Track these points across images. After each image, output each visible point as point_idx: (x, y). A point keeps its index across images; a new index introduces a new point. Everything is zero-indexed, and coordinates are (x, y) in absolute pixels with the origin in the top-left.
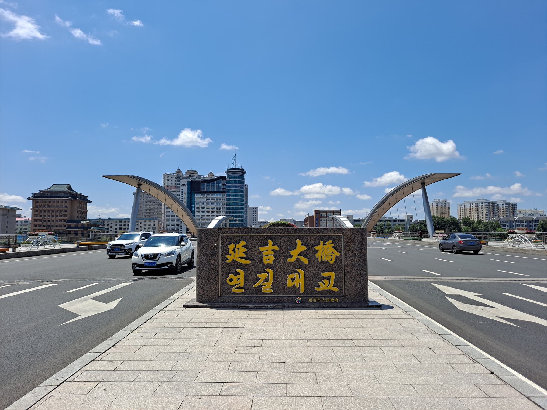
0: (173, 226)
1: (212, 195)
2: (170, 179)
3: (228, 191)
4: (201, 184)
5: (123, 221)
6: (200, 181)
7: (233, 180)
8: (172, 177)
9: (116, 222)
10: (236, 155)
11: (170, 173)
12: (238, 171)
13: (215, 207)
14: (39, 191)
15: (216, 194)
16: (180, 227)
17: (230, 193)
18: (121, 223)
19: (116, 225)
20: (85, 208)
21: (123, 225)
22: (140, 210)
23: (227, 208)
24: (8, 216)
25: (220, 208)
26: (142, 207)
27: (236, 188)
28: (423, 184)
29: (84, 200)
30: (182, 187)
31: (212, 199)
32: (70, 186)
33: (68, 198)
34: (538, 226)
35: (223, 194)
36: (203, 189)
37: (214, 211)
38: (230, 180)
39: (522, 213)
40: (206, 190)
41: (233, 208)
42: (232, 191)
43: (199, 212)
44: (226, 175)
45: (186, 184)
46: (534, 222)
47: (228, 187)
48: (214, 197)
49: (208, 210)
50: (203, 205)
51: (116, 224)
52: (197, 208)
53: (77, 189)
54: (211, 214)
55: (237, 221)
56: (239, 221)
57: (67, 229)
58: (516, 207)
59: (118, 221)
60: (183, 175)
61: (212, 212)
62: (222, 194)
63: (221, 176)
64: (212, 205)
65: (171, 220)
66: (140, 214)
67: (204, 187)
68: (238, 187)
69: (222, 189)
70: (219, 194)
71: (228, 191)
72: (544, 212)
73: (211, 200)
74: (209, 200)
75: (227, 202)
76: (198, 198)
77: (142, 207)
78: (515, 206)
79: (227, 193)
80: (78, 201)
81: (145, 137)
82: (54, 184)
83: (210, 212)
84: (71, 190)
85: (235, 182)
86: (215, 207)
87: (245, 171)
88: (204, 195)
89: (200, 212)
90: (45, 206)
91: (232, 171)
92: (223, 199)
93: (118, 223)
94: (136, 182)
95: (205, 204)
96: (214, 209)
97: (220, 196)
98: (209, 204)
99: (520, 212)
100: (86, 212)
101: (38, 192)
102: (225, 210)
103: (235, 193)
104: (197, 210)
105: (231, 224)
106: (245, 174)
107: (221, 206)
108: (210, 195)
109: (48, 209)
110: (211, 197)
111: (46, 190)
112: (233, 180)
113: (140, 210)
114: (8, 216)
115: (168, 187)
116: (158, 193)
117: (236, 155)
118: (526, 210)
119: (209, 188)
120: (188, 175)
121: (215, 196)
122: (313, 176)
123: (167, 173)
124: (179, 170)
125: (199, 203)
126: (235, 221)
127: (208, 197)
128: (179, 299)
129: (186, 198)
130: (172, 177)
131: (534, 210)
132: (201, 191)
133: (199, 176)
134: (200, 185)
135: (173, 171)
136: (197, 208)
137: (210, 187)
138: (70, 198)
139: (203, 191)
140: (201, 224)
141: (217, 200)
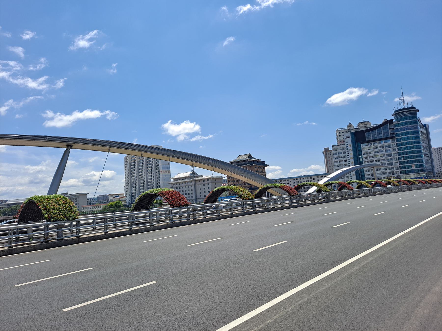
1: (380, 143)
2: (341, 134)
3: (398, 135)
4: (366, 133)
5: (286, 180)
6: (364, 130)
7: (402, 122)
8: (343, 132)
9: (294, 180)
10: (402, 93)
11: (341, 129)
12: (406, 110)
13: (384, 155)
15: (383, 141)
18: (297, 181)
19: (294, 183)
20: (264, 171)
22: (330, 166)
23: (399, 154)
24: (215, 184)
25: (391, 155)
26: (331, 163)
29: (262, 165)
30: (346, 140)
31: (380, 147)
32: (250, 155)
33: (247, 165)
35: (393, 139)
37: (384, 158)
38: (399, 122)
40: (372, 138)
41: (407, 153)
42: (403, 134)
43: (368, 162)
47: (398, 130)
48: (383, 144)
50: (371, 154)
51: (294, 181)
52: (365, 158)
53: (257, 156)
54: (381, 162)
55: (414, 167)
56: (416, 166)
59: (295, 179)
60: (354, 128)
61: (382, 160)
62: (391, 140)
64: (381, 153)
66: (330, 170)
69: (391, 134)
71: (398, 135)
74: (377, 148)
75: (398, 147)
76: (365, 148)
77: (331, 163)
79: (396, 138)
81: (58, 84)
82: (240, 155)
83: (380, 160)
84: (251, 158)
85: (406, 124)
86: (384, 155)
87: (417, 109)
88: (370, 144)
89: (369, 161)
91: (403, 111)
92: (393, 145)
93: (295, 181)
94: (65, 144)
95: (373, 153)
96: (384, 157)
98: (377, 152)
100: (265, 174)
102: (397, 157)
104: (366, 160)
105: (407, 171)
107: (392, 152)
108: (377, 143)
110: (378, 144)
111: (234, 161)
112: (402, 122)
113: (330, 166)
114: (215, 184)
115: (340, 142)
117: (402, 93)
120: (359, 127)
121: (383, 143)
123: (338, 129)
124: (350, 124)
125: (366, 153)
126: (411, 167)
127: (375, 145)
129: (352, 150)
130: (343, 132)
132: (366, 140)
133: (372, 126)
135: (345, 126)
136: (365, 158)
137: (376, 135)
138: (248, 164)
141: (386, 146)
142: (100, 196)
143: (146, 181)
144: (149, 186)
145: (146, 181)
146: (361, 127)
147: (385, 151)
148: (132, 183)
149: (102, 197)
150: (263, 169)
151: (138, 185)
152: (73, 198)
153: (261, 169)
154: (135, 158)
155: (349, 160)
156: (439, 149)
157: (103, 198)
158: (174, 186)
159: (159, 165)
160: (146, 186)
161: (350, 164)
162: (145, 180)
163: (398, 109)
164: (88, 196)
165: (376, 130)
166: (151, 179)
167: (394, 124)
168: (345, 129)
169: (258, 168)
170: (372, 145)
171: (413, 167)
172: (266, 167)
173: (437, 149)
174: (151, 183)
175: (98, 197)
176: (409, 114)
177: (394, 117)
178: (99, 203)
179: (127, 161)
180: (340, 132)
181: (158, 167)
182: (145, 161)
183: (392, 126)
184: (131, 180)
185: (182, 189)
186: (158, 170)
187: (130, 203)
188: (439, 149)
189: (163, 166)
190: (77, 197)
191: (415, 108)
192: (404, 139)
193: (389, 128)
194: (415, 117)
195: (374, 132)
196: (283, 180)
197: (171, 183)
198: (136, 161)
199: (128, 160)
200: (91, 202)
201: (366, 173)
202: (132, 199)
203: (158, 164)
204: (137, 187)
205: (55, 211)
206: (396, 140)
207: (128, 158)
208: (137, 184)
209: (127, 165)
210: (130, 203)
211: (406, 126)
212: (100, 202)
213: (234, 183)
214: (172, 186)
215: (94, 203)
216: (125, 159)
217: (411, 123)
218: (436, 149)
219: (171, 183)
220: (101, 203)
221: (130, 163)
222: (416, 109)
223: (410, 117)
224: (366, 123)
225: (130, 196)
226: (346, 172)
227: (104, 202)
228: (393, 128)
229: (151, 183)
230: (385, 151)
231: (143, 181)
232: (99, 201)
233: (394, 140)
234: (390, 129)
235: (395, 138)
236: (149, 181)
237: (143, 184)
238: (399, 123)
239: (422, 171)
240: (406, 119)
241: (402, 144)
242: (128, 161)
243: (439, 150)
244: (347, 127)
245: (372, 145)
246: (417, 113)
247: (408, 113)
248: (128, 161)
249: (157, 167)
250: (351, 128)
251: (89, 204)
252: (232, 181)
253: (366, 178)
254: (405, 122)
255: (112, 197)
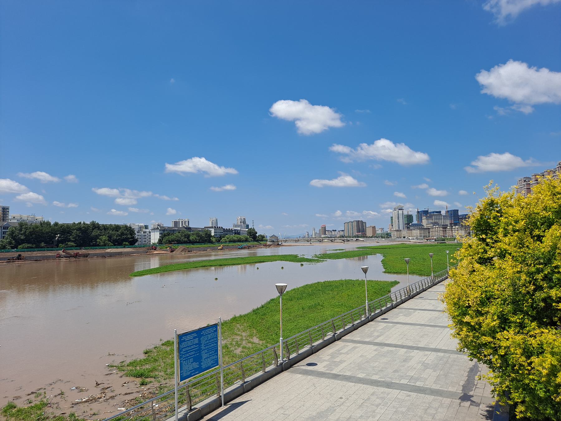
34: (7, 233)
39: (16, 219)
46: (3, 229)
49: (338, 409)
58: (8, 212)
72: (42, 218)
78: (7, 210)
79: (524, 306)
99: (14, 217)
118: (21, 216)
128: (19, 386)
131: (31, 216)
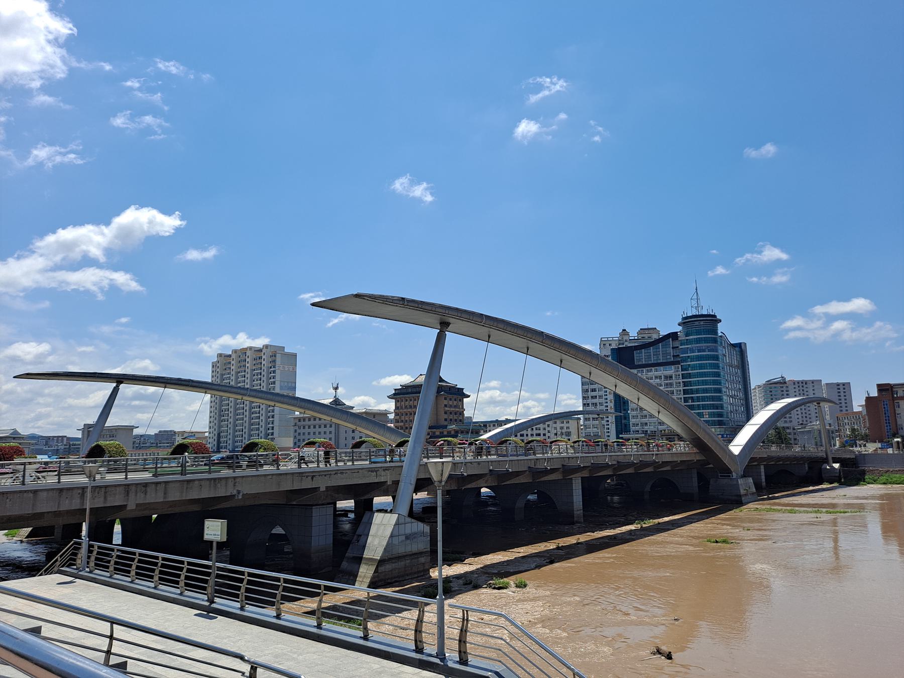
0: (596, 429)
3: (685, 360)
4: (635, 352)
6: (632, 346)
7: (691, 337)
10: (696, 289)
11: (608, 338)
12: (699, 319)
14: (401, 386)
15: (662, 368)
16: (606, 431)
17: (688, 363)
20: (460, 406)
21: (542, 429)
27: (698, 352)
28: (444, 326)
31: (656, 377)
35: (677, 366)
36: (640, 360)
38: (687, 338)
40: (645, 361)
42: (692, 359)
44: (679, 329)
45: (610, 354)
48: (660, 372)
55: (707, 416)
56: (711, 415)
57: (430, 438)
60: (631, 338)
63: (670, 333)
65: (591, 419)
67: (641, 357)
68: (704, 351)
70: (667, 366)
71: (685, 360)
73: (654, 378)
75: (683, 380)
79: (682, 364)
80: (444, 397)
82: (421, 375)
85: (698, 341)
88: (642, 371)
90: (406, 407)
97: (671, 371)
101: (400, 387)
102: (682, 396)
103: (697, 362)
106: (718, 324)
108: (652, 370)
109: (405, 410)
116: (590, 370)
117: (696, 289)
119: (649, 357)
120: (640, 338)
122: (253, 339)
123: (601, 338)
124: (624, 330)
132: (636, 363)
134: (634, 353)
139: (640, 363)
140: (641, 423)
141: (666, 377)
142: (160, 432)
143: (248, 411)
144: (252, 419)
145: (248, 411)
146: (642, 338)
147: (663, 385)
148: (222, 413)
149: (164, 434)
150: (459, 402)
151: (232, 418)
152: (107, 435)
153: (455, 403)
154: (233, 365)
155: (606, 397)
156: (802, 383)
157: (165, 436)
158: (298, 423)
159: (274, 383)
160: (247, 419)
161: (607, 402)
162: (247, 408)
163: (688, 315)
164: (136, 432)
165: (652, 348)
166: (258, 407)
167: (680, 340)
168: (614, 339)
169: (451, 400)
170: (644, 373)
171: (705, 416)
172: (465, 400)
173: (798, 383)
174: (258, 415)
175: (156, 434)
176: (703, 325)
177: (681, 327)
178: (157, 447)
179: (216, 371)
180: (605, 343)
181: (272, 385)
182: (250, 372)
183: (677, 344)
184: (221, 406)
185: (314, 430)
186: (274, 374)
187: (214, 450)
188: (802, 383)
189: (282, 384)
190: (114, 432)
191: (714, 316)
192: (694, 367)
193: (671, 346)
194: (715, 332)
195: (649, 351)
196: (498, 424)
197: (293, 417)
198: (232, 371)
199: (218, 368)
200: (140, 443)
201: (632, 421)
202: (219, 442)
203: (273, 414)
204: (231, 420)
205: (114, 452)
206: (682, 368)
207: (218, 365)
208: (231, 415)
209: (216, 377)
210: (215, 450)
211: (697, 345)
212: (159, 445)
213: (404, 425)
214: (295, 423)
215: (146, 446)
216: (213, 366)
217: (706, 340)
218: (796, 383)
219: (294, 418)
220: (161, 446)
221: (222, 375)
222: (716, 318)
223: (705, 331)
224: (651, 331)
225: (216, 438)
226: (535, 421)
227: (168, 446)
228: (678, 347)
229: (258, 415)
230: (663, 385)
231: (242, 411)
232: (157, 443)
233: (678, 368)
234: (673, 348)
235: (679, 364)
236: (253, 410)
237: (242, 416)
238: (687, 340)
239: (720, 423)
240: (698, 333)
241: (690, 375)
242: (218, 370)
243: (801, 385)
244: (619, 336)
245: (644, 373)
246: (718, 324)
247: (702, 323)
248: (218, 370)
249: (271, 386)
250: (626, 338)
251: (137, 447)
252: (402, 421)
253: (631, 430)
254: (696, 338)
255: (182, 438)
